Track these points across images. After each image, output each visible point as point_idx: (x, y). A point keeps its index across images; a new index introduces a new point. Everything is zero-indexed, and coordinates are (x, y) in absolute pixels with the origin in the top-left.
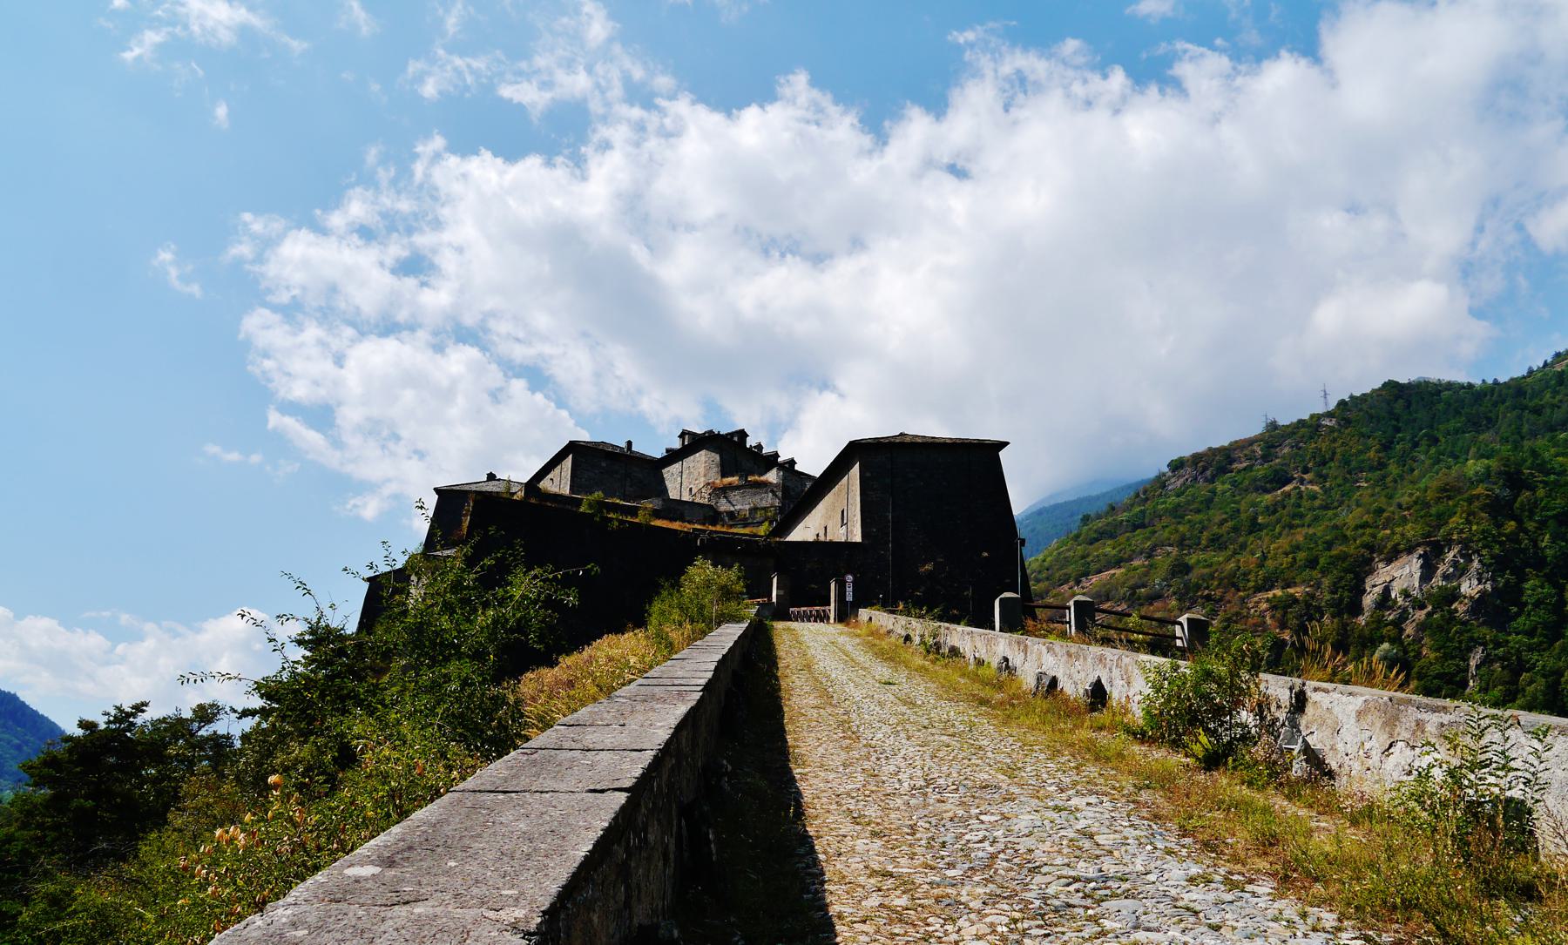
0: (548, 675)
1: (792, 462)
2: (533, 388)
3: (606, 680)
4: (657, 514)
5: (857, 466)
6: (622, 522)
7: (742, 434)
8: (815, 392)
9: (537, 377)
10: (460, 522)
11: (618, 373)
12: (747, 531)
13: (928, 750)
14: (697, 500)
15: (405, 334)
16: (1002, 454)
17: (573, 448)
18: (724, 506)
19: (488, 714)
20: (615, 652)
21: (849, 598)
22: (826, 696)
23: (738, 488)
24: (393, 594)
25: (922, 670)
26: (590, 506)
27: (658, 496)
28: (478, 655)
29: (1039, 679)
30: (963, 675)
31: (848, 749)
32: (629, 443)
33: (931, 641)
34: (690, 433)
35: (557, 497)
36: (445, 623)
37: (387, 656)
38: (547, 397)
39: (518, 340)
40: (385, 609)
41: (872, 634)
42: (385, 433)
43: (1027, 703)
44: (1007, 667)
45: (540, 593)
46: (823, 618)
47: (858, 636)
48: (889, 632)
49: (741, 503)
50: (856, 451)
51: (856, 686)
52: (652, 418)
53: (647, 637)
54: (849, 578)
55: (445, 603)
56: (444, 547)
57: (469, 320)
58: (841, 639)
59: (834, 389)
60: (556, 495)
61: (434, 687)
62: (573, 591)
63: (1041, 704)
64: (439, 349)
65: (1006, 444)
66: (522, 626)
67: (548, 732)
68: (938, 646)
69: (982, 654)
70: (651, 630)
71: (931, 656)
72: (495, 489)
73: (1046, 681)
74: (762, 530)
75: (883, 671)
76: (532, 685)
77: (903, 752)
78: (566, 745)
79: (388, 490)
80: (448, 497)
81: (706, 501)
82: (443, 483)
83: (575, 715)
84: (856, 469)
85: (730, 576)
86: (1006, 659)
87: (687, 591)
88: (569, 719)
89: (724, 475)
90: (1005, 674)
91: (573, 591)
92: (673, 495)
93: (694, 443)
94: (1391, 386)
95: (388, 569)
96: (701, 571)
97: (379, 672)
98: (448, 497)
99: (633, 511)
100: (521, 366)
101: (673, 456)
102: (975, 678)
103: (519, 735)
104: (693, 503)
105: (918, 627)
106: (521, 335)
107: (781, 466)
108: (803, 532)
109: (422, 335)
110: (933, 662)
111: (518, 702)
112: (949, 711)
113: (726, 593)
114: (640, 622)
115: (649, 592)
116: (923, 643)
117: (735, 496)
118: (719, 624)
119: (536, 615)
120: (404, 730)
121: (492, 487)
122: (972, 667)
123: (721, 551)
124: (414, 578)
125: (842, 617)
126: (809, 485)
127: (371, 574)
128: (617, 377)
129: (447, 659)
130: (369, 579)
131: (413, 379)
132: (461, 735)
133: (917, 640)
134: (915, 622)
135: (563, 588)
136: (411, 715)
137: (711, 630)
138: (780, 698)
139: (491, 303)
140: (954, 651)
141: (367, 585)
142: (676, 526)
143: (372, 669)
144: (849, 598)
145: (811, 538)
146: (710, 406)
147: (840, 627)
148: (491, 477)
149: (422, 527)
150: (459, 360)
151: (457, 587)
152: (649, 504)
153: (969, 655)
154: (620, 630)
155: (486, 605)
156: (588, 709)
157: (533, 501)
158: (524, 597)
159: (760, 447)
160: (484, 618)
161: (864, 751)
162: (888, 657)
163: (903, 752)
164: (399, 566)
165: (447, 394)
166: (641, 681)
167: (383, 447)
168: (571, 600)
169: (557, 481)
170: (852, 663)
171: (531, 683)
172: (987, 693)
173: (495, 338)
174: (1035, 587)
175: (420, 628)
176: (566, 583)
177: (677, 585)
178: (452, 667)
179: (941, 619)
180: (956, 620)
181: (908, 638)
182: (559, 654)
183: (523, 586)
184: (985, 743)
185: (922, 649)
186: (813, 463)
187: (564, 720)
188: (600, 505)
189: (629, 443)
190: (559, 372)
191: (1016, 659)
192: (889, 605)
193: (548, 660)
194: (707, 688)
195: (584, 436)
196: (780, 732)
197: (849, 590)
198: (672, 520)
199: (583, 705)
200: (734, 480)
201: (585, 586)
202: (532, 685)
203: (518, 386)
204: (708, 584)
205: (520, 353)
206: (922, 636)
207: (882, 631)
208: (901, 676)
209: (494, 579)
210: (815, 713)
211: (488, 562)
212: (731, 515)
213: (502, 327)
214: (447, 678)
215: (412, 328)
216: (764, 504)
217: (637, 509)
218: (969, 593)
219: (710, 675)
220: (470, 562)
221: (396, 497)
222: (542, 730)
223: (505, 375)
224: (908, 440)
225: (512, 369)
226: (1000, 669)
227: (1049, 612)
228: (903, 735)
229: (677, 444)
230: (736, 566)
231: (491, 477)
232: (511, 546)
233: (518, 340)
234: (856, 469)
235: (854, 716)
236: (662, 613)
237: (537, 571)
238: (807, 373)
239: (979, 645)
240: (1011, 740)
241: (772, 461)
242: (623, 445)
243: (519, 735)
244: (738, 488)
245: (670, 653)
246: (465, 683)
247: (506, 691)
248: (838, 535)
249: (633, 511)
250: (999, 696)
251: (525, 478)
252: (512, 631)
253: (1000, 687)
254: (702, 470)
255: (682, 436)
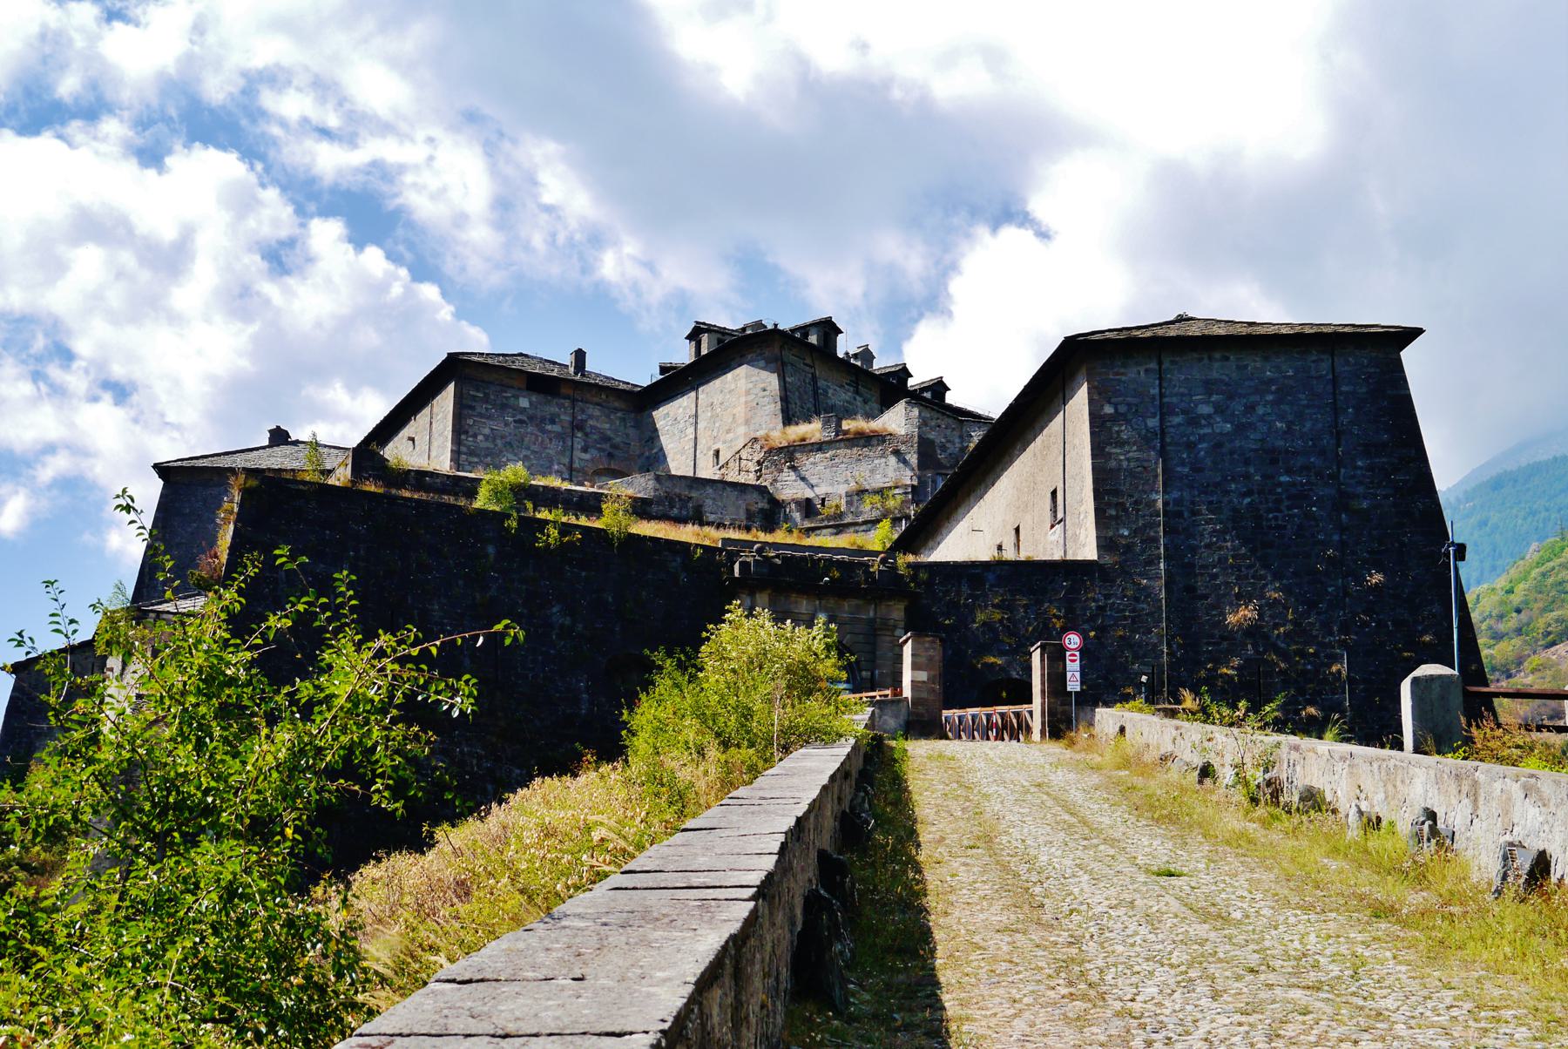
0: (405, 868)
1: (939, 388)
2: (358, 240)
3: (541, 880)
4: (641, 509)
5: (1084, 389)
6: (566, 529)
7: (829, 329)
8: (982, 231)
9: (369, 212)
10: (213, 542)
11: (547, 199)
12: (843, 541)
13: (1261, 1021)
14: (732, 476)
15: (74, 127)
16: (1405, 355)
17: (454, 368)
18: (789, 488)
19: (281, 959)
20: (558, 817)
21: (1074, 685)
22: (1027, 900)
23: (820, 447)
24: (70, 698)
25: (1239, 841)
26: (496, 494)
27: (645, 469)
28: (260, 829)
29: (1507, 857)
30: (1335, 851)
31: (1081, 1021)
32: (580, 356)
33: (1258, 777)
34: (710, 329)
35: (421, 478)
36: (185, 759)
37: (56, 835)
38: (391, 256)
39: (325, 133)
40: (50, 733)
41: (1126, 763)
42: (40, 343)
43: (1483, 911)
44: (1434, 831)
45: (392, 689)
46: (1015, 730)
47: (1096, 769)
48: (1164, 759)
49: (828, 479)
50: (1075, 358)
51: (1095, 880)
52: (633, 297)
53: (628, 782)
54: (1073, 640)
55: (187, 717)
56: (184, 592)
57: (216, 89)
58: (1059, 778)
59: (1024, 219)
60: (421, 474)
61: (162, 904)
62: (467, 685)
63: (1512, 915)
64: (151, 156)
65: (1418, 332)
66: (354, 765)
67: (418, 996)
68: (1275, 789)
69: (1376, 804)
70: (637, 766)
71: (1261, 811)
72: (289, 464)
73: (1524, 862)
74: (879, 538)
75: (1153, 846)
76: (380, 892)
77: (1204, 1027)
78: (458, 1026)
79: (50, 469)
80: (186, 485)
81: (750, 479)
82: (172, 451)
83: (476, 958)
84: (1080, 401)
85: (809, 641)
86: (1432, 816)
87: (713, 677)
88: (461, 969)
89: (788, 419)
90: (1430, 847)
91: (467, 685)
92: (678, 464)
93: (721, 351)
94: (1067, 339)
95: (60, 643)
96: (745, 634)
97: (39, 872)
98: (186, 485)
99: (591, 505)
100: (335, 190)
101: (675, 382)
102: (1363, 858)
103: (354, 1006)
104: (723, 483)
105: (1235, 745)
106: (333, 121)
107: (915, 397)
108: (968, 540)
109: (112, 127)
110: (1265, 824)
111: (352, 928)
112: (1303, 932)
113: (803, 682)
114: (612, 749)
115: (633, 680)
116: (1241, 780)
117: (814, 465)
118: (786, 749)
119: (385, 741)
120: (95, 1003)
121: (279, 459)
122: (1354, 832)
123: (790, 583)
124: (114, 662)
125: (1058, 728)
126: (977, 436)
127: (20, 656)
128: (549, 209)
129: (192, 841)
130: (17, 668)
131: (94, 227)
132: (222, 1008)
133: (1227, 775)
134: (1219, 733)
135: (444, 675)
136: (112, 968)
137: (768, 762)
138: (923, 910)
139: (268, 51)
140: (1312, 800)
141: (10, 680)
142: (687, 534)
143: (24, 867)
144: (1074, 685)
145: (985, 554)
146: (752, 267)
147: (1055, 748)
148: (279, 437)
149: (127, 546)
150: (207, 171)
151: (212, 681)
152: (639, 486)
153: (1346, 806)
154: (567, 766)
155: (272, 719)
156: (504, 943)
157: (370, 487)
158: (353, 698)
159: (866, 355)
160: (271, 748)
161: (1116, 1027)
162: (1165, 814)
163: (1204, 1027)
164: (84, 634)
165: (171, 259)
166: (617, 879)
167: (37, 376)
168: (461, 701)
169: (422, 440)
170: (1079, 827)
171: (384, 887)
172: (1391, 890)
173: (276, 131)
174: (1490, 652)
175: (131, 772)
176: (449, 664)
177: (690, 667)
178: (206, 856)
179: (1279, 726)
180: (1314, 728)
181: (1206, 772)
182: (436, 823)
183: (352, 671)
184: (1390, 1003)
185: (1239, 796)
186: (986, 389)
187: (450, 970)
188: (522, 492)
189: (580, 356)
190: (420, 203)
191: (1453, 816)
192: (1159, 697)
193: (411, 836)
194: (766, 891)
195: (477, 341)
196: (926, 989)
197: (1073, 669)
198: (680, 520)
199: (493, 934)
200: (813, 430)
201: (492, 667)
202: (380, 892)
203: (326, 235)
204: (758, 662)
205: (329, 160)
206: (1239, 767)
207: (1150, 757)
208: (1194, 858)
209: (292, 660)
210: (1002, 943)
211: (276, 622)
212: (808, 507)
213: (291, 105)
214: (193, 886)
215: (92, 109)
216: (878, 481)
217: (598, 498)
218: (1341, 668)
219: (769, 863)
220: (240, 625)
221: (70, 485)
222: (403, 992)
223: (300, 211)
224: (1194, 330)
225: (310, 197)
226: (1418, 837)
227: (1524, 708)
228: (1202, 988)
229: (683, 355)
230: (821, 619)
231: (279, 437)
232: (325, 586)
233: (325, 133)
234: (1080, 401)
235: (1091, 948)
236: (660, 730)
237: (385, 640)
238: (972, 181)
239: (1368, 785)
240: (1448, 997)
241: (893, 386)
242: (567, 359)
243: (354, 1006)
244: (820, 447)
245: (681, 814)
246: (231, 894)
247: (329, 907)
248: (1044, 546)
249: (591, 505)
250: (1415, 899)
251: (354, 439)
252: (331, 773)
253: (1420, 877)
254: (740, 411)
255: (695, 335)
